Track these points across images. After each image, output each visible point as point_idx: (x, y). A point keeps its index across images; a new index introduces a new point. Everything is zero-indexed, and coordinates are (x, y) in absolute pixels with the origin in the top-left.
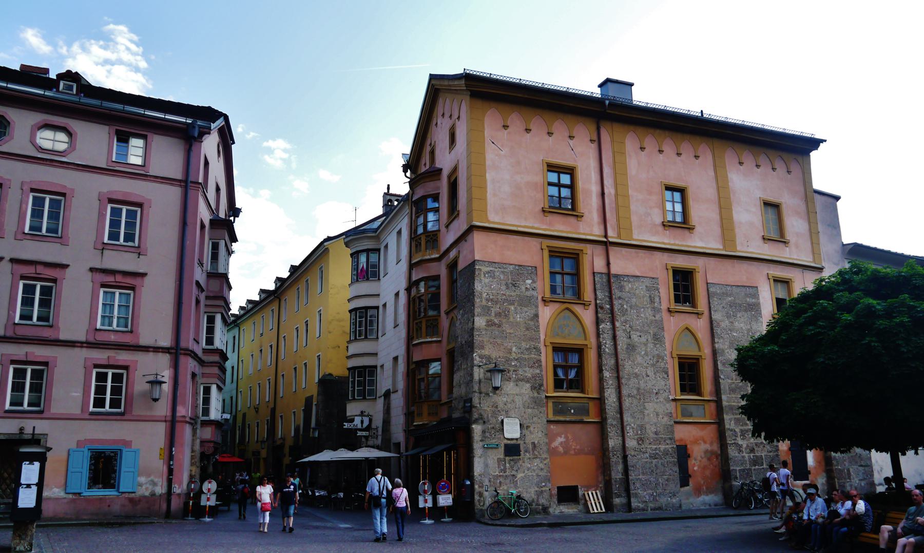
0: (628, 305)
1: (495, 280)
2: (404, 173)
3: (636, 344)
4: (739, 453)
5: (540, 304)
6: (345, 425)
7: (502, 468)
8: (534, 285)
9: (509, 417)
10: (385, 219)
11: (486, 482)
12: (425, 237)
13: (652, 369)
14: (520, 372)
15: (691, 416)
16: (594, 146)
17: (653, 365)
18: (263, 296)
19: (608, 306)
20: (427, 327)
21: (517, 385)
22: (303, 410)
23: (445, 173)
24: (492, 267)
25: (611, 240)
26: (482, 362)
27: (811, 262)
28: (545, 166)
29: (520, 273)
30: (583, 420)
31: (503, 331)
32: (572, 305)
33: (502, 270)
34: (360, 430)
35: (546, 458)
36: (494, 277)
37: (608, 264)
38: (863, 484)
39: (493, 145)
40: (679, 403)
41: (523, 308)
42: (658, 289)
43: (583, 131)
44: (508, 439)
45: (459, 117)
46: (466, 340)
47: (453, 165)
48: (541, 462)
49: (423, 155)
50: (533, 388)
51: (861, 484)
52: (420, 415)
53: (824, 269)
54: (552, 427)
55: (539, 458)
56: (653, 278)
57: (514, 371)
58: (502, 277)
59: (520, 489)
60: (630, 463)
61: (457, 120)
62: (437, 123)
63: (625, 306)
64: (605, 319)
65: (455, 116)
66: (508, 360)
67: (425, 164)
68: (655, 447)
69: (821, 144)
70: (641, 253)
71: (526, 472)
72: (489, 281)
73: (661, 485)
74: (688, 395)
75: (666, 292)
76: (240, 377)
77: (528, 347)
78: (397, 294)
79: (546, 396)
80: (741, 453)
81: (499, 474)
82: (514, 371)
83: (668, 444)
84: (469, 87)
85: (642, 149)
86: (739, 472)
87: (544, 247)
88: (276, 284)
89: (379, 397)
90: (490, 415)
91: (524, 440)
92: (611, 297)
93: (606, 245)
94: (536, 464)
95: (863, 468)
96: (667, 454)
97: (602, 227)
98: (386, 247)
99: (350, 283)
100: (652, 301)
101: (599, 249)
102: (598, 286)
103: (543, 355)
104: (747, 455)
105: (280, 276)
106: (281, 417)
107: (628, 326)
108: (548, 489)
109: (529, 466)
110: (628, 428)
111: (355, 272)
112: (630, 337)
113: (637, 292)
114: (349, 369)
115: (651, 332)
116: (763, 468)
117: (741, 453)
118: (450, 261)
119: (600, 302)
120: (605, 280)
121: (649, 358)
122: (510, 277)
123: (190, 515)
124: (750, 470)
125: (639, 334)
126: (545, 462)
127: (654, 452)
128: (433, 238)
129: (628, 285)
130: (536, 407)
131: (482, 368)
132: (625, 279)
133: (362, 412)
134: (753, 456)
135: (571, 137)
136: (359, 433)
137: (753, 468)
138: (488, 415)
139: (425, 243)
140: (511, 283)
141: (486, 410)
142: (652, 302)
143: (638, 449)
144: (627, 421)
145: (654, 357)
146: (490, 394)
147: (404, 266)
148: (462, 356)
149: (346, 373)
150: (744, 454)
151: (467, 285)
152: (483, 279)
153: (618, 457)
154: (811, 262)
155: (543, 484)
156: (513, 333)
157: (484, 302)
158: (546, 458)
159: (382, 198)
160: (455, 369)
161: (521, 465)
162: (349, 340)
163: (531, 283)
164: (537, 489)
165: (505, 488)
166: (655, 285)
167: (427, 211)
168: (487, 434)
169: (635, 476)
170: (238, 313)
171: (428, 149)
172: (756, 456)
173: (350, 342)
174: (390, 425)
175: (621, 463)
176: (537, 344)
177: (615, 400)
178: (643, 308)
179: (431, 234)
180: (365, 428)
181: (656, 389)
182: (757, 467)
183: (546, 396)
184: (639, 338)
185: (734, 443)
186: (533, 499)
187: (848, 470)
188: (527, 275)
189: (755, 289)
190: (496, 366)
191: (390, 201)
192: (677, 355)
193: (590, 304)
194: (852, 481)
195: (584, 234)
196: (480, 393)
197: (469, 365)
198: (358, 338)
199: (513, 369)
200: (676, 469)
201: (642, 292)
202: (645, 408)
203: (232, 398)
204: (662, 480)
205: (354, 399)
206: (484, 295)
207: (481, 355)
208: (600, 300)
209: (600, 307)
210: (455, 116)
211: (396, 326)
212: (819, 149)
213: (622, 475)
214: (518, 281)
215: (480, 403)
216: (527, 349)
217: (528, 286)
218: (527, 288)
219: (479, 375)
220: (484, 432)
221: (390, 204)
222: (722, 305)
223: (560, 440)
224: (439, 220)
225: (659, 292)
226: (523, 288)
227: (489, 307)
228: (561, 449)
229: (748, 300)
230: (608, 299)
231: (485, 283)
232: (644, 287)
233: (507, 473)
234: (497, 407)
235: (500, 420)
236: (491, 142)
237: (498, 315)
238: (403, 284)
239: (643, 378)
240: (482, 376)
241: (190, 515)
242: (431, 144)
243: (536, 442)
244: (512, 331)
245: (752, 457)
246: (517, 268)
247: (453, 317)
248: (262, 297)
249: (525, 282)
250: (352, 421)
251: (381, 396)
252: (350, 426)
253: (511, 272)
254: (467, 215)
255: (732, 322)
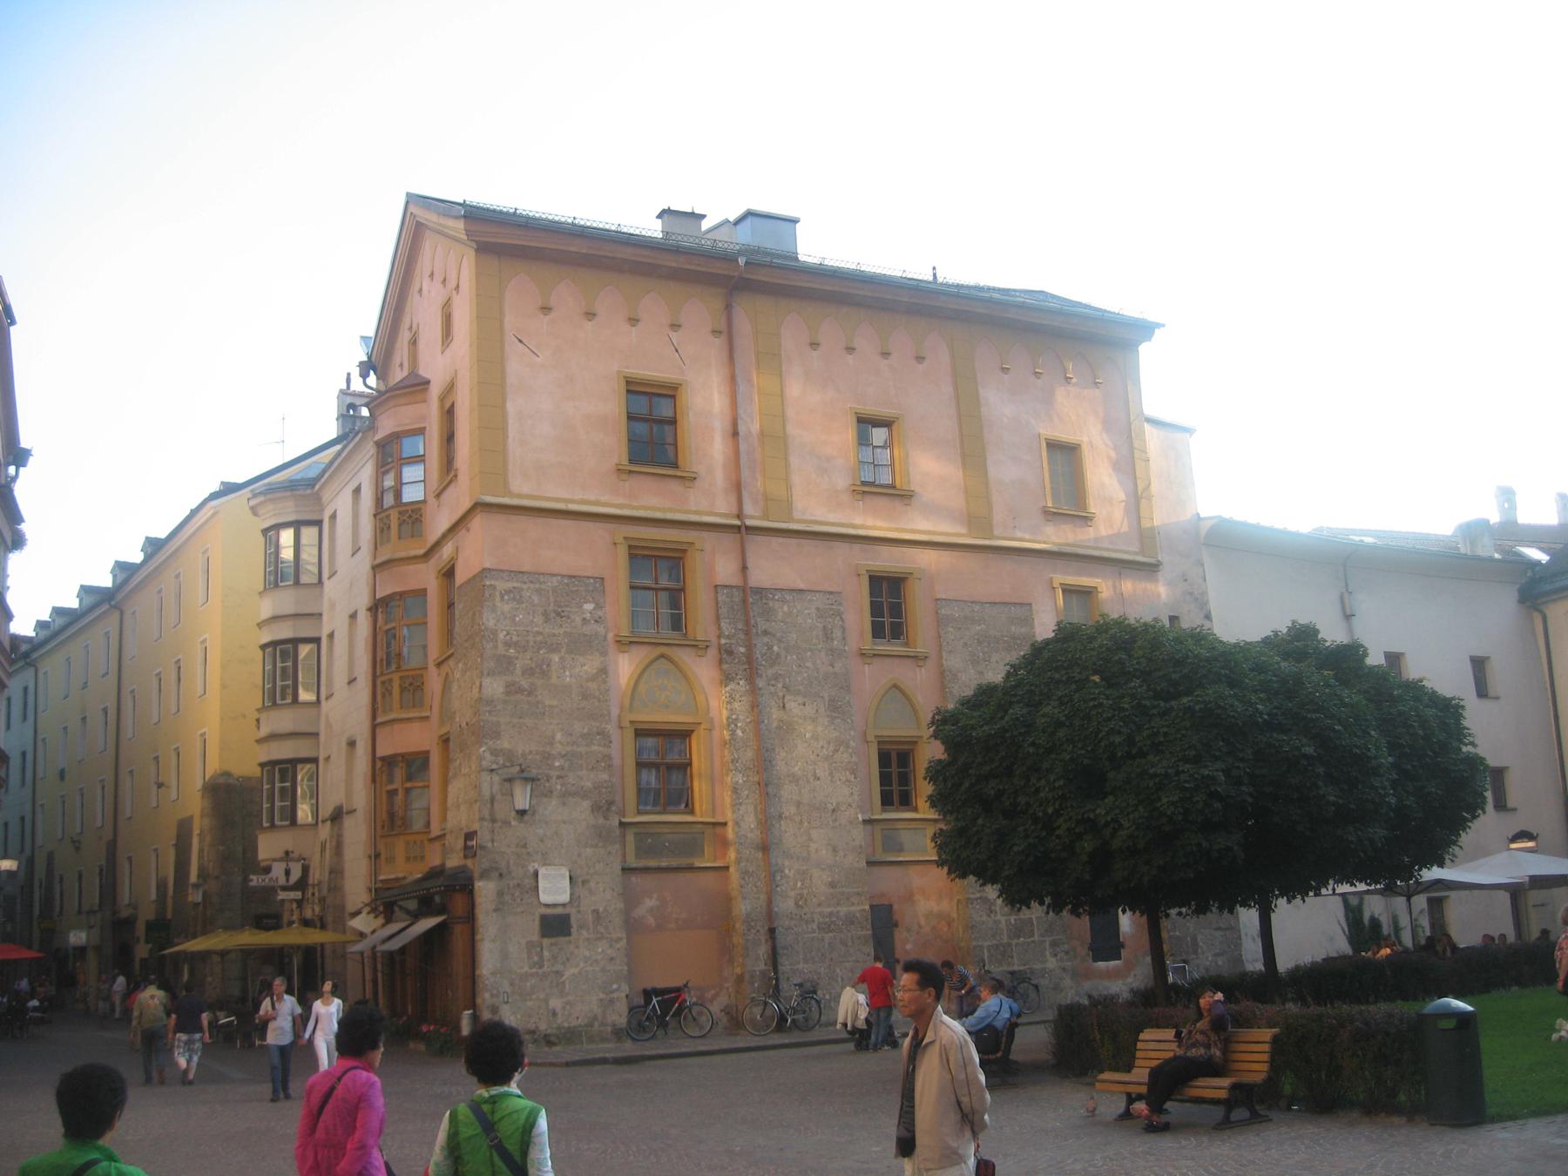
0: (782, 645)
1: (524, 606)
2: (361, 379)
3: (796, 719)
4: (989, 916)
5: (612, 648)
6: (252, 880)
7: (536, 959)
8: (600, 613)
9: (550, 865)
10: (339, 453)
11: (506, 986)
12: (397, 515)
13: (827, 766)
14: (571, 779)
15: (901, 850)
16: (719, 342)
17: (827, 758)
18: (89, 600)
19: (742, 650)
20: (403, 690)
21: (564, 804)
22: (173, 845)
23: (435, 391)
24: (517, 581)
25: (749, 522)
26: (497, 764)
27: (1136, 553)
28: (623, 384)
29: (572, 592)
30: (693, 864)
31: (538, 702)
32: (676, 649)
33: (537, 586)
34: (284, 888)
35: (620, 939)
36: (520, 602)
37: (744, 568)
38: (1220, 963)
39: (520, 344)
40: (878, 828)
41: (577, 656)
42: (840, 614)
43: (700, 311)
44: (547, 906)
45: (458, 286)
46: (468, 720)
47: (448, 379)
48: (611, 946)
49: (398, 345)
50: (596, 808)
51: (1216, 963)
52: (391, 860)
53: (1161, 567)
54: (633, 879)
55: (607, 938)
56: (831, 593)
57: (559, 777)
58: (536, 599)
59: (570, 998)
60: (781, 940)
61: (454, 292)
62: (421, 290)
63: (775, 648)
64: (737, 675)
65: (452, 284)
66: (547, 757)
67: (401, 365)
68: (829, 910)
69: (1156, 330)
70: (807, 544)
71: (582, 965)
72: (512, 608)
73: (840, 979)
74: (897, 810)
75: (857, 616)
76: (40, 774)
77: (585, 731)
78: (353, 616)
79: (620, 821)
80: (992, 915)
81: (529, 971)
82: (559, 777)
83: (853, 904)
84: (472, 235)
85: (814, 345)
86: (989, 951)
87: (620, 539)
88: (115, 577)
89: (323, 822)
90: (511, 862)
91: (578, 906)
92: (747, 633)
93: (741, 531)
94: (600, 950)
95: (1222, 933)
96: (852, 923)
97: (733, 499)
98: (333, 517)
99: (262, 589)
100: (828, 635)
101: (728, 540)
102: (724, 611)
103: (616, 746)
104: (1003, 919)
105: (122, 559)
106: (130, 859)
107: (780, 685)
108: (623, 995)
109: (587, 954)
110: (779, 878)
111: (272, 568)
112: (784, 707)
113: (800, 620)
114: (262, 765)
115: (826, 695)
116: (1033, 942)
117: (992, 915)
118: (443, 565)
119: (728, 641)
120: (737, 600)
121: (821, 743)
122: (552, 600)
123: (660, 998)
124: (1009, 945)
125: (800, 699)
126: (618, 946)
127: (827, 920)
128: (412, 516)
129: (782, 608)
130: (600, 845)
131: (497, 773)
132: (776, 597)
133: (287, 853)
134: (1015, 920)
135: (675, 326)
136: (282, 895)
137: (1016, 941)
138: (508, 863)
139: (396, 524)
140: (555, 611)
141: (504, 853)
142: (827, 638)
143: (796, 915)
144: (777, 864)
145: (829, 743)
146: (513, 823)
147: (364, 560)
148: (461, 751)
149: (257, 771)
150: (999, 917)
151: (470, 614)
152: (499, 604)
153: (758, 931)
154: (1136, 553)
155: (615, 986)
156: (557, 706)
157: (501, 650)
158: (620, 939)
159: (336, 400)
160: (451, 774)
161: (572, 953)
162: (260, 706)
163: (594, 609)
164: (602, 996)
165: (542, 996)
166: (833, 607)
167: (403, 462)
168: (507, 898)
169: (791, 965)
170: (33, 634)
171: (404, 337)
172: (1020, 919)
173: (263, 709)
174: (343, 878)
175: (763, 941)
176: (603, 726)
177: (752, 826)
178: (811, 650)
179: (409, 508)
180: (295, 884)
181: (832, 804)
182: (1022, 939)
183: (620, 821)
184: (802, 707)
185: (981, 898)
186: (596, 1015)
187: (1194, 939)
188: (584, 594)
189: (1028, 608)
190: (522, 771)
191: (352, 406)
192: (876, 736)
193: (707, 646)
194: (1201, 956)
195: (696, 512)
196: (494, 821)
197: (473, 768)
198: (279, 702)
199: (557, 773)
200: (868, 950)
201: (810, 621)
202: (810, 839)
203: (23, 819)
204: (841, 970)
205: (273, 826)
206: (501, 636)
207: (496, 749)
208: (728, 637)
209: (726, 651)
210: (452, 284)
211: (352, 681)
212: (1153, 339)
213: (766, 964)
214: (567, 606)
215: (493, 841)
216: (583, 736)
217: (588, 616)
218: (584, 619)
219: (491, 788)
220: (500, 894)
221: (351, 412)
222: (962, 641)
223: (650, 903)
224: (424, 481)
225: (842, 619)
226: (578, 620)
227: (509, 657)
228: (651, 921)
229: (1013, 628)
230: (742, 636)
231: (503, 613)
232: (813, 610)
233: (545, 969)
234: (525, 846)
235: (532, 870)
236: (516, 341)
237: (528, 672)
238: (362, 601)
239: (808, 782)
240: (496, 787)
241: (660, 998)
242: (411, 328)
243: (601, 909)
244: (554, 703)
245: (1013, 922)
246: (566, 581)
247: (447, 674)
248: (84, 602)
249: (581, 607)
250: (267, 870)
251: (326, 820)
252: (263, 880)
253: (554, 590)
254: (471, 479)
255: (981, 673)
